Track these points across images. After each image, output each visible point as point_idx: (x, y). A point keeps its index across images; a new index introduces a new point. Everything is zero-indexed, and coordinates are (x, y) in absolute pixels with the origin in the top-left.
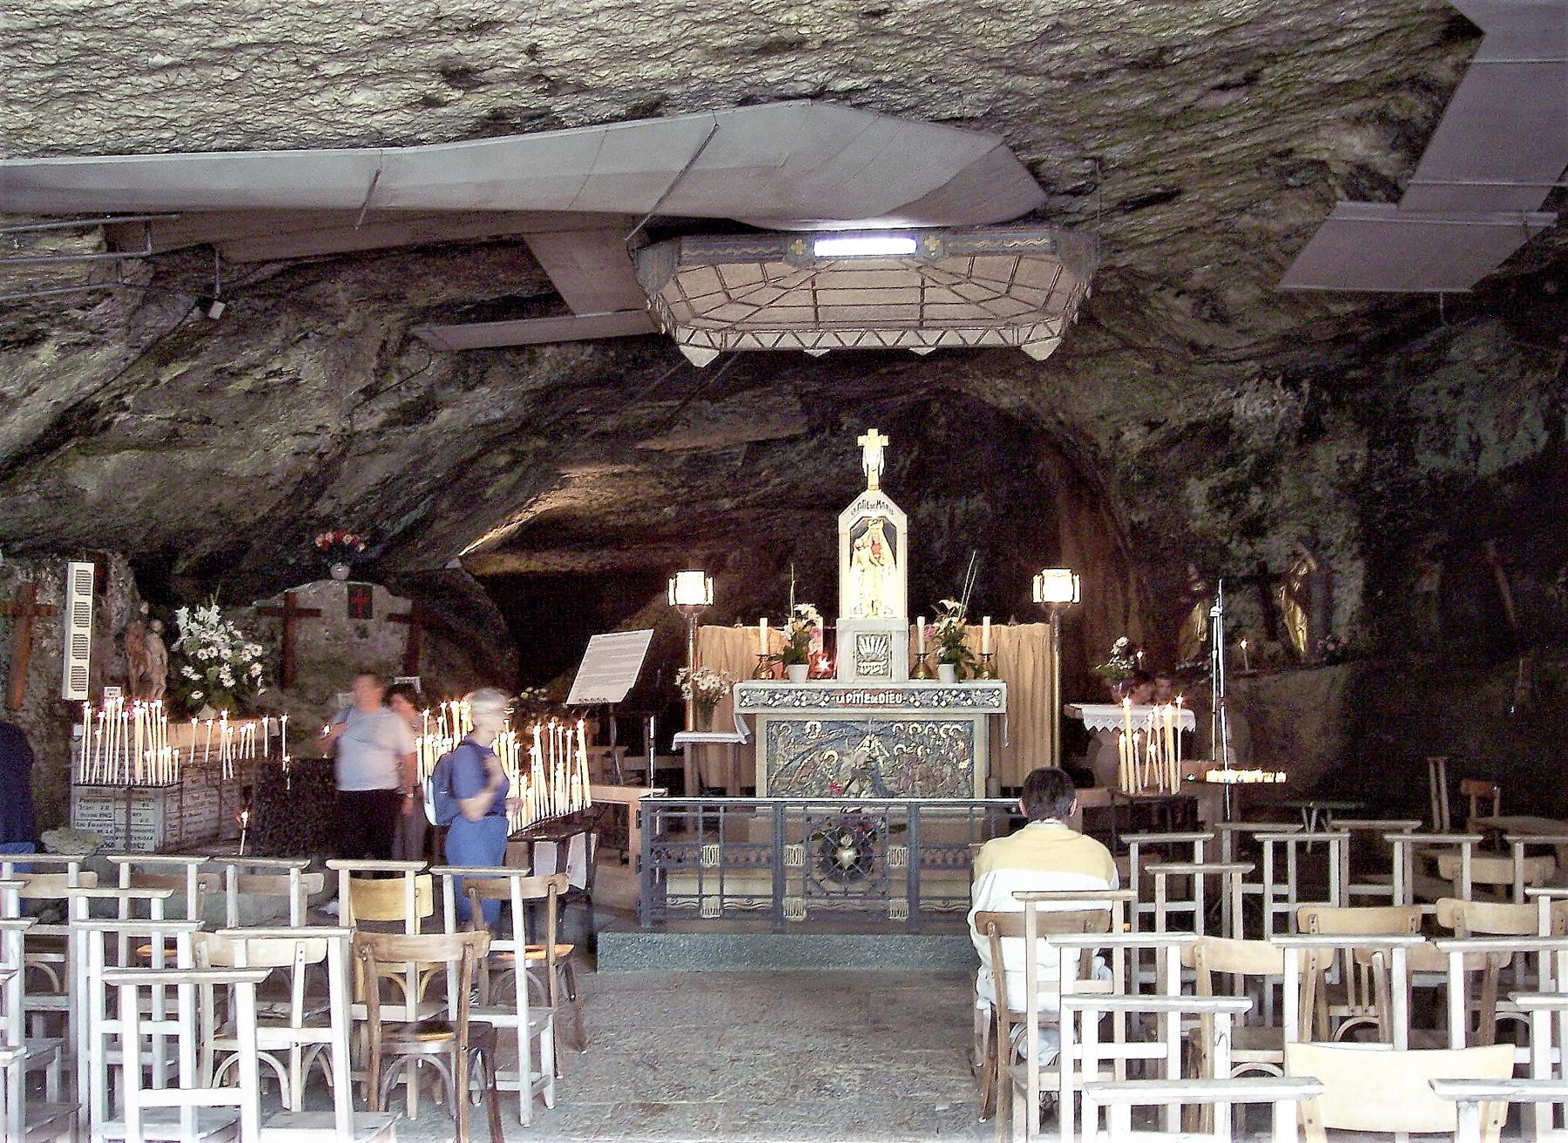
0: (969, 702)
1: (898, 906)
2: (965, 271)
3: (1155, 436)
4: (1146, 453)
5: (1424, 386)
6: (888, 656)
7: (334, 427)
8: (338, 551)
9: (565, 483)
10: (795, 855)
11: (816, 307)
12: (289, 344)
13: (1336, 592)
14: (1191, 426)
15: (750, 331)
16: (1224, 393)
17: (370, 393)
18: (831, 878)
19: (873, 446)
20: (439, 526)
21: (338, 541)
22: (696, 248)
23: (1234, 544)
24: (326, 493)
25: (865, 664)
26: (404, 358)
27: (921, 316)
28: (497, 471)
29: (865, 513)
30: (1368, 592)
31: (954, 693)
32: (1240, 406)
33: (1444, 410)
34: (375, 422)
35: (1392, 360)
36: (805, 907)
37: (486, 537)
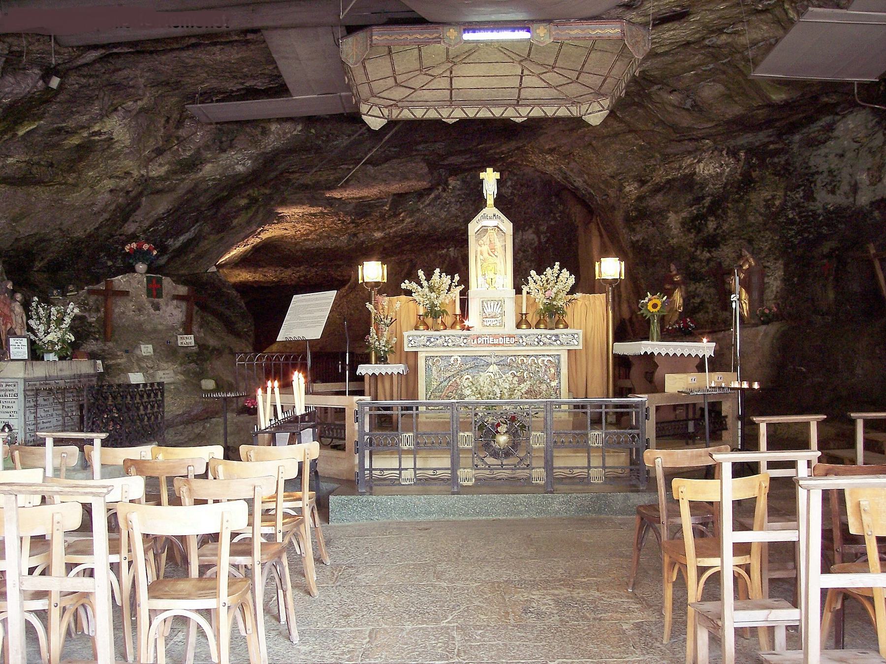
0: (558, 342)
1: (538, 474)
2: (552, 63)
3: (645, 188)
4: (640, 198)
5: (819, 152)
6: (503, 314)
7: (135, 173)
8: (140, 255)
9: (281, 219)
10: (467, 439)
11: (451, 90)
12: (105, 114)
13: (766, 280)
14: (668, 181)
15: (407, 107)
16: (689, 161)
17: (159, 152)
18: (491, 455)
19: (490, 178)
20: (204, 245)
21: (140, 249)
22: (383, 35)
23: (698, 252)
24: (131, 219)
25: (488, 319)
26: (181, 130)
27: (519, 97)
28: (240, 210)
29: (486, 223)
30: (786, 280)
31: (548, 336)
32: (700, 168)
33: (832, 166)
34: (163, 171)
35: (797, 137)
36: (473, 476)
37: (232, 253)
